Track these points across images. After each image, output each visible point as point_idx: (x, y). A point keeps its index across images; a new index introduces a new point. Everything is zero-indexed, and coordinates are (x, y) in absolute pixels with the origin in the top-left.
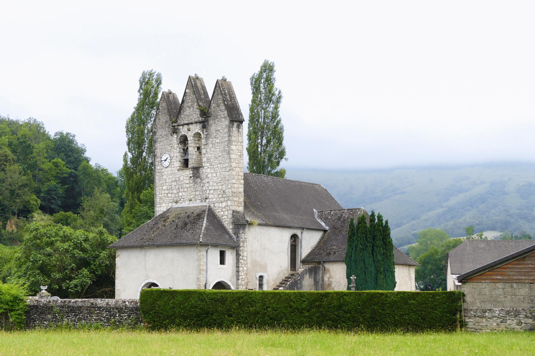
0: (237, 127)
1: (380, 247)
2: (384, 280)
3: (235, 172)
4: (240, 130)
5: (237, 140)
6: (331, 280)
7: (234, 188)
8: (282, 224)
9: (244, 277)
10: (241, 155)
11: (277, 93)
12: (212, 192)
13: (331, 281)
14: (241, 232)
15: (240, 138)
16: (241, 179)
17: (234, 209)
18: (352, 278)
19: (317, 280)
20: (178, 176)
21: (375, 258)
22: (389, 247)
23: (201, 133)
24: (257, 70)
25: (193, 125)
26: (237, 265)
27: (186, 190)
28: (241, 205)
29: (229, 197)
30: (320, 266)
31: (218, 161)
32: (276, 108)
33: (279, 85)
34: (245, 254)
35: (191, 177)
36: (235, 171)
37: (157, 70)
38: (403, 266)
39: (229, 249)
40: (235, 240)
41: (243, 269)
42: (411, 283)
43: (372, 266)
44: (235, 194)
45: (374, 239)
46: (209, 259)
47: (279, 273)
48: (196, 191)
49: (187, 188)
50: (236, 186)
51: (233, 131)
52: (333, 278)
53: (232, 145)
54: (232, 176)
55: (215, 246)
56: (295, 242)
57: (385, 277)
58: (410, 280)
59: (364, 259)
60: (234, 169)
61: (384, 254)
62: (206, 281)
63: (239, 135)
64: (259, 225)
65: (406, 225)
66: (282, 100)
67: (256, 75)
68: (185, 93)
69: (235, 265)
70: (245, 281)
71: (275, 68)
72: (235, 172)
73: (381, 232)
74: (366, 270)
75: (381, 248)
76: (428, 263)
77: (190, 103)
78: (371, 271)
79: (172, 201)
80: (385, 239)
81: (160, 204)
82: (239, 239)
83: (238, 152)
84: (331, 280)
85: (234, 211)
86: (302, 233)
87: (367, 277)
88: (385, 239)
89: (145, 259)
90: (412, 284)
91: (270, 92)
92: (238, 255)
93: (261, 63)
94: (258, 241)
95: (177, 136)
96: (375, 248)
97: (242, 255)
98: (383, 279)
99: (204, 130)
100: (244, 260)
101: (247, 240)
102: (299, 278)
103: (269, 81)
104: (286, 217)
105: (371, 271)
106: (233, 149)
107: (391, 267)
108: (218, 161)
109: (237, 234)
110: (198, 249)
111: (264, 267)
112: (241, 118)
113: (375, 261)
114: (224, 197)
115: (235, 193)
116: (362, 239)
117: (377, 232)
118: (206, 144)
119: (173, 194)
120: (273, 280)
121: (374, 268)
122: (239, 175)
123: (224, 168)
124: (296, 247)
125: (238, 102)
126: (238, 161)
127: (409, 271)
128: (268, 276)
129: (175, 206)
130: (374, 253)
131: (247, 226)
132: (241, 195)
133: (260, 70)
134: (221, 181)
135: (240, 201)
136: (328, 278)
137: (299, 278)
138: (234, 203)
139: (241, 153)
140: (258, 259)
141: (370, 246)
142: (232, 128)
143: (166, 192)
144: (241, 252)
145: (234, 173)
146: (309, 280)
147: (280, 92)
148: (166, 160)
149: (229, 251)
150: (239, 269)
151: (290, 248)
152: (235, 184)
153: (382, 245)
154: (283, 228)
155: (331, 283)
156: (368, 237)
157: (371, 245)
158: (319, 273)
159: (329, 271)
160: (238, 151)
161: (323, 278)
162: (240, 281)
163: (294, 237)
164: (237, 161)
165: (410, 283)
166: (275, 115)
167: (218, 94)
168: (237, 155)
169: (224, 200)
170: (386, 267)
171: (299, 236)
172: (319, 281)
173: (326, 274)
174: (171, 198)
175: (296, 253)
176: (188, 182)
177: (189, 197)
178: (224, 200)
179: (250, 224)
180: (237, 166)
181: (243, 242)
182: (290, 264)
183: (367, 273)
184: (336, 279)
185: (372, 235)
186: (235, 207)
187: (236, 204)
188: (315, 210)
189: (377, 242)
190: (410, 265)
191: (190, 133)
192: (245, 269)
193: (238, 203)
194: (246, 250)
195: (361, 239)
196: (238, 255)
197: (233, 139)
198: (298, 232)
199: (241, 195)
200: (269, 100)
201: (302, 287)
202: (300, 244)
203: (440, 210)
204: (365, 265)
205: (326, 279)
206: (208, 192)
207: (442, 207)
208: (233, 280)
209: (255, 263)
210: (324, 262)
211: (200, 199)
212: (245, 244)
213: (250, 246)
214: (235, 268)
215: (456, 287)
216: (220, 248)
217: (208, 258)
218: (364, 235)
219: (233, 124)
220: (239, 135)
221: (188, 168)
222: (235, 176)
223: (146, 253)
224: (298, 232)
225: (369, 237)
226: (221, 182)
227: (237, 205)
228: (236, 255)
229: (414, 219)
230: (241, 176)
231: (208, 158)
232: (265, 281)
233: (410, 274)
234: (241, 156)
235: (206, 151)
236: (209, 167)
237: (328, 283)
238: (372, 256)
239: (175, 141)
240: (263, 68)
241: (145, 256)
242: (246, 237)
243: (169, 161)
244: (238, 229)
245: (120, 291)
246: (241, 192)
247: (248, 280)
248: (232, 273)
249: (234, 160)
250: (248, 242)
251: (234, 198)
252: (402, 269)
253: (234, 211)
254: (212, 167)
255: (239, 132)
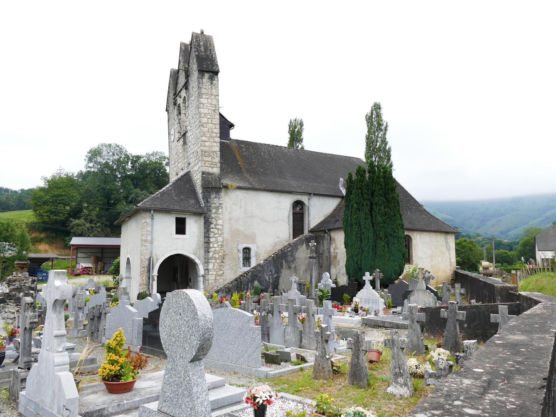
0: (209, 78)
1: (380, 206)
2: (386, 249)
3: (207, 129)
4: (214, 82)
5: (209, 93)
6: (336, 251)
7: (205, 146)
8: (279, 188)
9: (217, 249)
10: (215, 110)
11: (385, 124)
13: (337, 253)
14: (213, 197)
15: (214, 91)
16: (216, 137)
17: (204, 170)
18: (311, 245)
19: (321, 252)
21: (374, 221)
22: (393, 205)
24: (369, 111)
26: (207, 235)
28: (215, 166)
30: (324, 236)
32: (385, 134)
33: (386, 117)
34: (220, 222)
36: (206, 127)
37: (299, 118)
38: (437, 234)
39: (191, 216)
40: (203, 205)
41: (217, 240)
42: (449, 254)
43: (370, 230)
44: (206, 154)
45: (373, 195)
46: (155, 227)
47: (276, 245)
50: (207, 144)
51: (203, 82)
52: (338, 248)
53: (202, 98)
54: (202, 133)
55: (167, 211)
56: (303, 210)
57: (388, 245)
58: (449, 249)
59: (359, 222)
60: (205, 125)
61: (386, 214)
62: (151, 254)
63: (212, 87)
64: (239, 188)
65: (520, 228)
66: (388, 128)
67: (368, 113)
69: (203, 235)
70: (221, 254)
71: (382, 106)
72: (207, 129)
73: (381, 185)
74: (362, 237)
75: (382, 207)
76: (527, 245)
78: (369, 236)
80: (388, 194)
82: (209, 204)
83: (211, 107)
84: (336, 251)
85: (203, 173)
86: (309, 199)
87: (363, 245)
88: (388, 194)
90: (451, 255)
91: (380, 125)
92: (207, 224)
93: (372, 104)
94: (241, 207)
96: (374, 206)
97: (215, 223)
98: (384, 246)
100: (218, 229)
101: (223, 206)
102: (289, 249)
103: (379, 116)
104: (293, 184)
105: (369, 236)
106: (203, 102)
107: (397, 231)
109: (207, 199)
111: (252, 238)
112: (215, 69)
113: (375, 225)
115: (206, 152)
116: (357, 197)
117: (376, 186)
120: (265, 253)
121: (372, 233)
122: (212, 132)
124: (304, 215)
125: (215, 54)
126: (211, 116)
127: (446, 239)
128: (258, 247)
130: (373, 213)
131: (223, 190)
132: (215, 155)
133: (371, 109)
135: (213, 161)
136: (334, 249)
137: (289, 249)
138: (205, 163)
139: (215, 107)
140: (241, 228)
141: (367, 205)
142: (202, 79)
144: (214, 220)
145: (205, 130)
146: (307, 251)
147: (387, 123)
149: (191, 218)
150: (209, 240)
151: (292, 216)
152: (207, 142)
153: (384, 202)
154: (280, 194)
155: (337, 255)
156: (364, 193)
157: (369, 203)
158: (323, 243)
159: (335, 241)
160: (211, 105)
161: (329, 249)
162: (211, 254)
163: (298, 204)
164: (208, 117)
165: (448, 254)
166: (384, 142)
168: (209, 109)
170: (389, 230)
171: (305, 202)
172: (323, 253)
173: (332, 244)
175: (303, 223)
179: (226, 187)
180: (210, 122)
181: (217, 208)
182: (292, 233)
183: (363, 239)
184: (341, 249)
185: (370, 191)
186: (207, 168)
187: (207, 164)
188: (341, 179)
189: (376, 198)
190: (447, 233)
192: (220, 239)
193: (212, 164)
194: (221, 217)
195: (356, 197)
196: (207, 224)
197: (204, 91)
198: (304, 199)
199: (215, 155)
200: (379, 128)
201: (295, 260)
202: (307, 212)
203: (541, 219)
204: (361, 229)
205: (332, 250)
207: (542, 217)
208: (198, 253)
209: (236, 234)
210: (330, 230)
212: (220, 210)
213: (227, 213)
214: (202, 239)
215: (542, 260)
216: (175, 214)
217: (154, 228)
218: (360, 191)
219: (203, 75)
220: (212, 87)
222: (206, 133)
224: (304, 199)
225: (366, 193)
227: (209, 165)
228: (205, 223)
229: (525, 224)
230: (216, 133)
232: (253, 253)
233: (447, 243)
234: (216, 111)
237: (334, 254)
238: (369, 217)
240: (373, 108)
242: (221, 202)
244: (208, 193)
246: (215, 152)
247: (224, 253)
248: (197, 244)
249: (204, 115)
250: (224, 209)
251: (204, 157)
252: (435, 237)
253: (203, 173)
255: (212, 84)
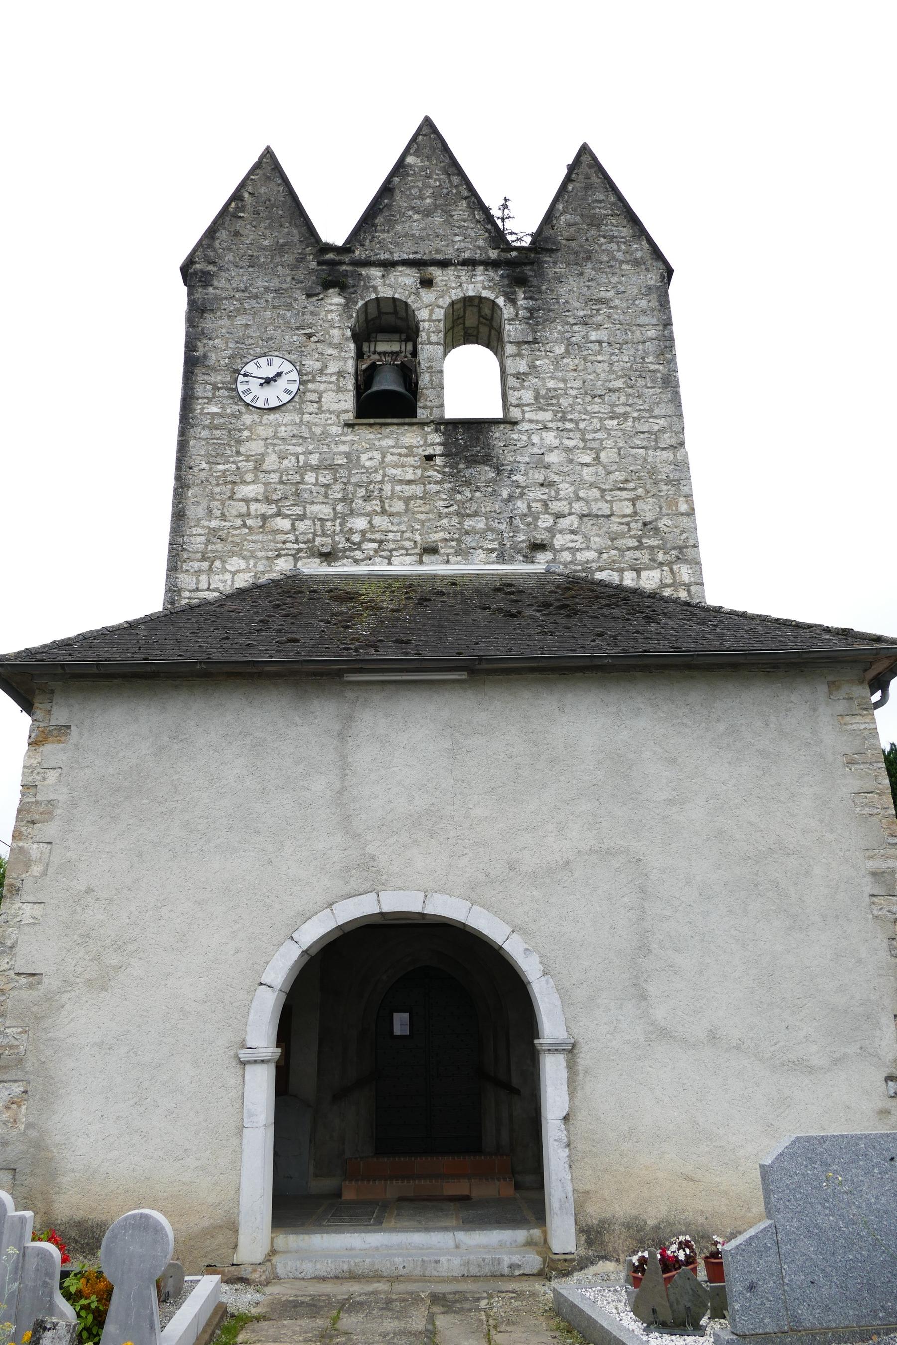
12: (572, 521)
20: (344, 448)
23: (501, 301)
25: (451, 271)
27: (399, 506)
29: (680, 549)
31: (605, 409)
35: (429, 458)
48: (462, 515)
49: (407, 500)
68: (400, 167)
77: (428, 201)
79: (300, 551)
81: (204, 559)
89: (343, 757)
95: (347, 307)
99: (514, 293)
108: (605, 409)
110: (842, 693)
114: (651, 548)
118: (530, 339)
119: (308, 522)
123: (642, 436)
129: (312, 567)
134: (627, 481)
143: (262, 508)
148: (268, 381)
167: (588, 187)
169: (653, 560)
174: (291, 537)
176: (412, 477)
177: (418, 538)
178: (653, 560)
191: (428, 296)
206: (545, 521)
211: (492, 551)
221: (414, 420)
223: (350, 719)
226: (631, 485)
231: (543, 392)
235: (532, 366)
236: (550, 425)
239: (334, 316)
241: (342, 737)
243: (293, 388)
245: (50, 983)
254: (569, 426)
